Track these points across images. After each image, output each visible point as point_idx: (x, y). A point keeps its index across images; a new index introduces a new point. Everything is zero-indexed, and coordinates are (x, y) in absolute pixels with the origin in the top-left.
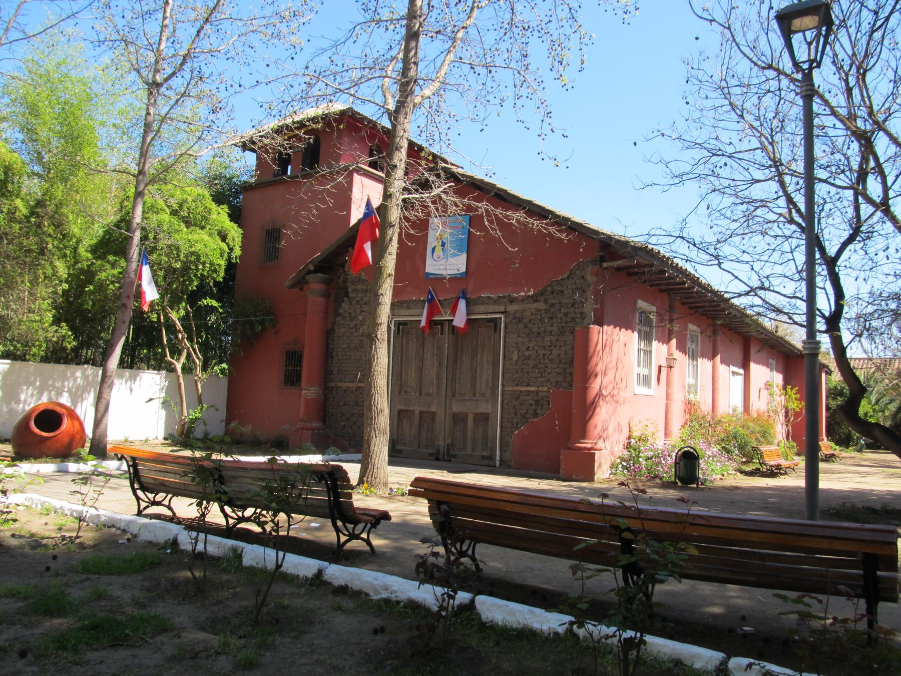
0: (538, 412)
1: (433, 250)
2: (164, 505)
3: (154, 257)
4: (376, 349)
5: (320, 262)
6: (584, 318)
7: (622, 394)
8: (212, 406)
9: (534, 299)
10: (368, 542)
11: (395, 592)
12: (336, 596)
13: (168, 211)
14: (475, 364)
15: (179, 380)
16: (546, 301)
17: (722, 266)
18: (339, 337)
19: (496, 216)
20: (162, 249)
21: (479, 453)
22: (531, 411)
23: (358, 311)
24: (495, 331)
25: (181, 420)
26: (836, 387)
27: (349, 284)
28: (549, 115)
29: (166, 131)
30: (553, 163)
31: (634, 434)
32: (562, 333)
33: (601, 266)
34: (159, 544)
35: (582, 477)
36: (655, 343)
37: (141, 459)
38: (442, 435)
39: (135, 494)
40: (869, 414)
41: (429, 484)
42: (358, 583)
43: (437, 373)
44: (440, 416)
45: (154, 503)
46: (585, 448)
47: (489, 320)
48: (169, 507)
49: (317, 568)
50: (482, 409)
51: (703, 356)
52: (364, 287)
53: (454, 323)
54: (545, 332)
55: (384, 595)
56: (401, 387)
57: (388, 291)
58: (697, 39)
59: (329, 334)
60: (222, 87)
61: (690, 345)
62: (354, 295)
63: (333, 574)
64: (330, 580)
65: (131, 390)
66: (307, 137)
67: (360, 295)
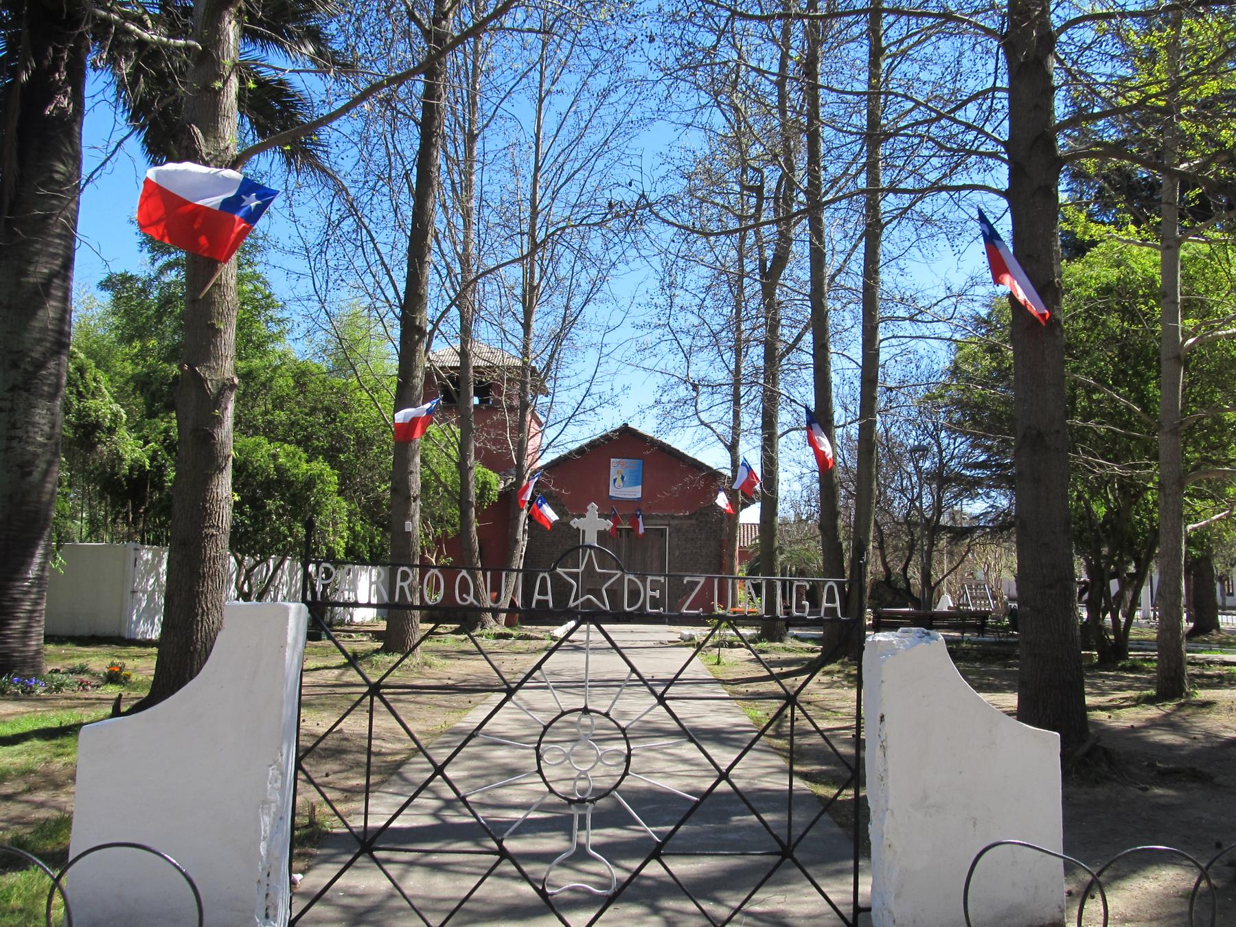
1: (615, 480)
9: (689, 517)
16: (697, 519)
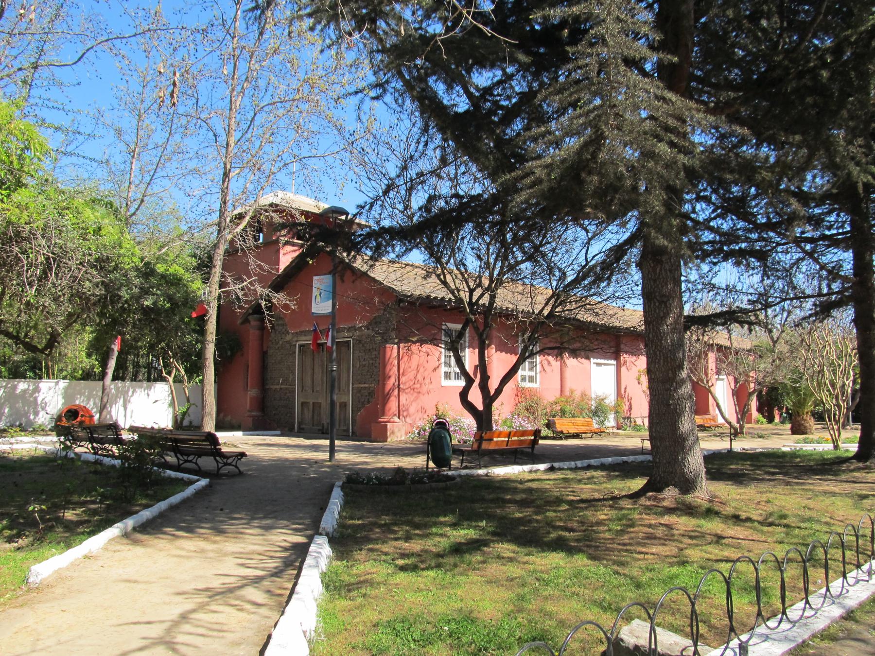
45: (186, 461)
50: (342, 400)
56: (303, 387)
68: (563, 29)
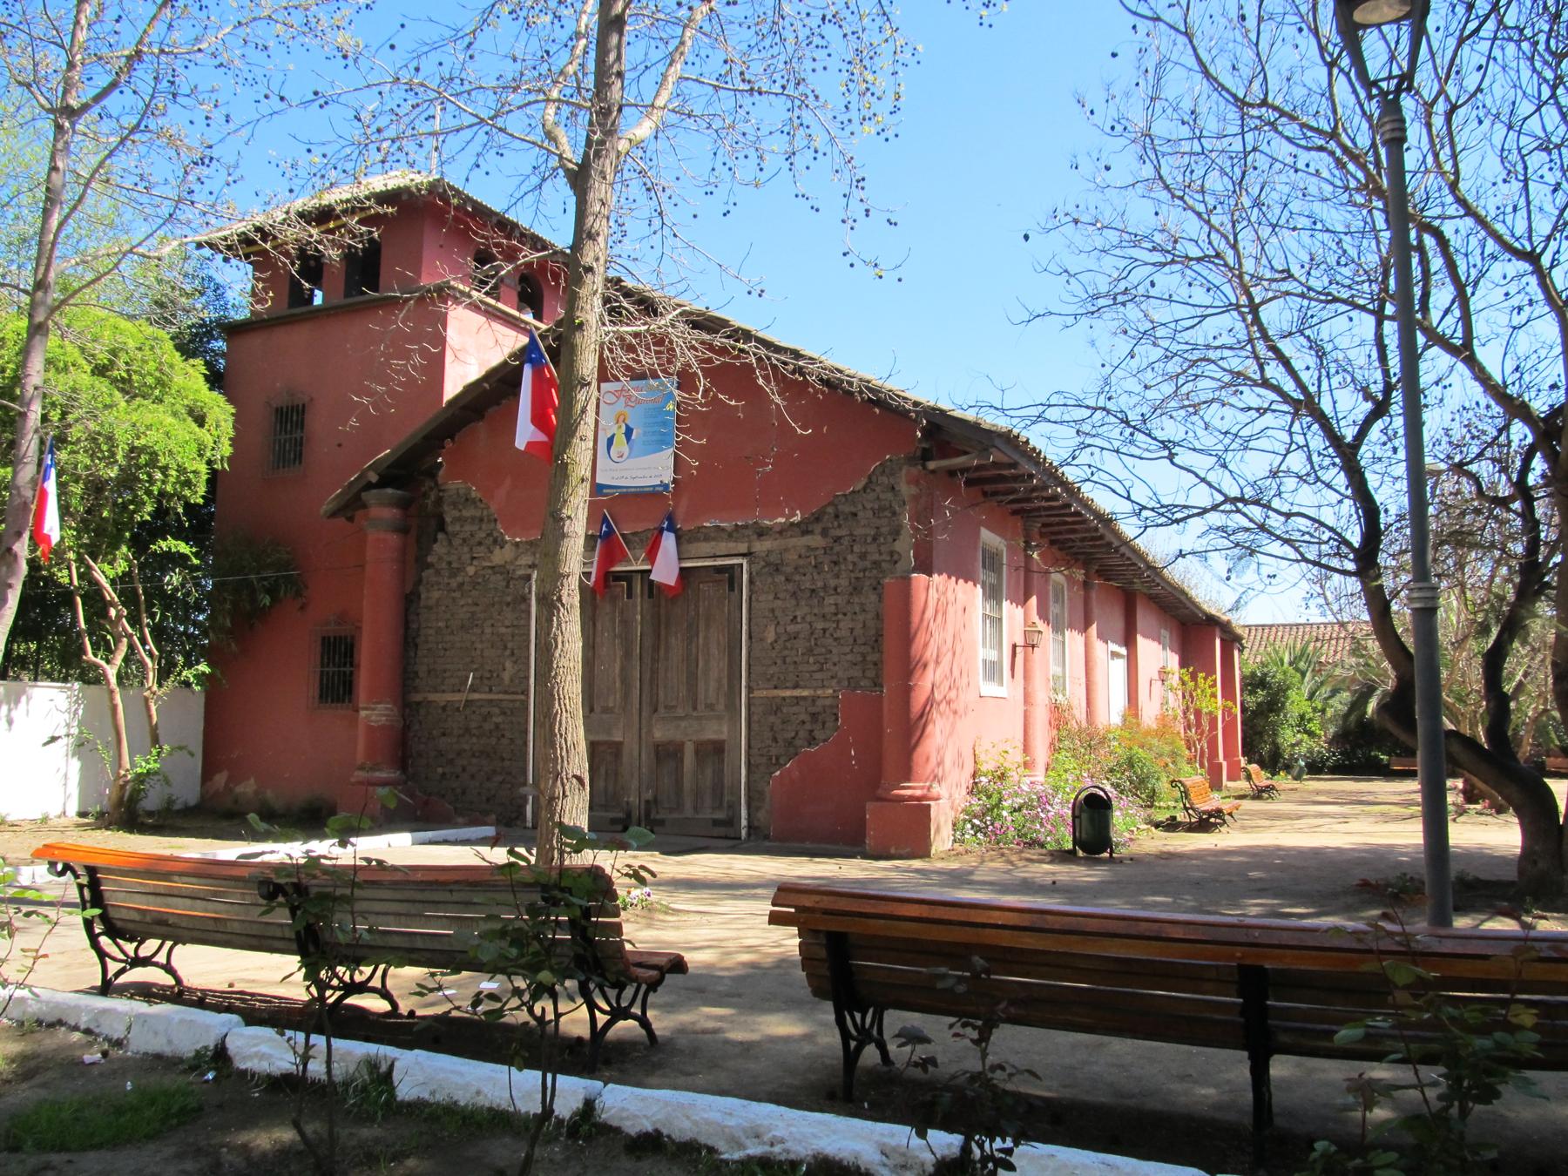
0: (817, 734)
1: (610, 441)
2: (157, 965)
3: (63, 455)
4: (559, 624)
5: (388, 467)
6: (896, 562)
7: (962, 696)
8: (181, 748)
9: (803, 529)
10: (644, 1022)
11: (782, 1141)
12: (639, 1159)
13: (88, 368)
14: (694, 650)
15: (112, 699)
16: (824, 533)
17: (1176, 460)
18: (430, 608)
19: (774, 367)
20: (79, 440)
21: (708, 814)
22: (802, 734)
23: (466, 557)
24: (732, 588)
25: (118, 777)
26: (1253, 674)
27: (446, 508)
28: (860, 184)
29: (98, 202)
30: (873, 272)
31: (984, 768)
32: (856, 590)
33: (924, 467)
34: (181, 1060)
35: (908, 850)
36: (1006, 604)
37: (110, 871)
38: (635, 784)
39: (95, 944)
40: (1307, 717)
41: (817, 898)
42: (686, 1124)
43: (623, 669)
44: (631, 749)
46: (912, 798)
47: (720, 570)
48: (168, 968)
49: (581, 1097)
51: (1071, 626)
52: (478, 514)
53: (652, 577)
54: (825, 587)
55: (755, 1150)
57: (580, 510)
58: (1114, 55)
59: (409, 601)
60: (218, 116)
61: (1054, 609)
62: (457, 528)
63: (623, 1109)
64: (615, 1123)
65: (10, 722)
66: (364, 229)
67: (468, 528)
68: (1440, 722)
